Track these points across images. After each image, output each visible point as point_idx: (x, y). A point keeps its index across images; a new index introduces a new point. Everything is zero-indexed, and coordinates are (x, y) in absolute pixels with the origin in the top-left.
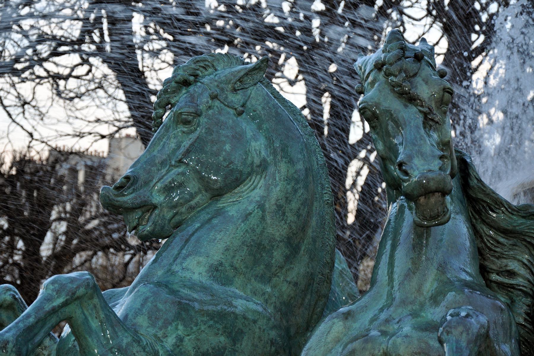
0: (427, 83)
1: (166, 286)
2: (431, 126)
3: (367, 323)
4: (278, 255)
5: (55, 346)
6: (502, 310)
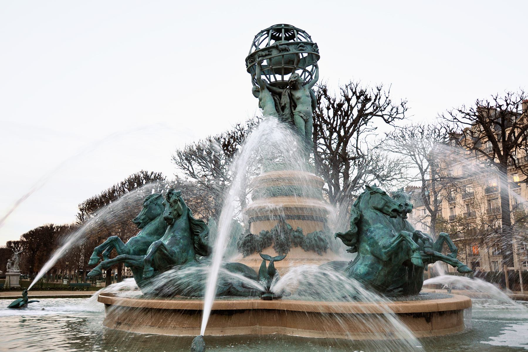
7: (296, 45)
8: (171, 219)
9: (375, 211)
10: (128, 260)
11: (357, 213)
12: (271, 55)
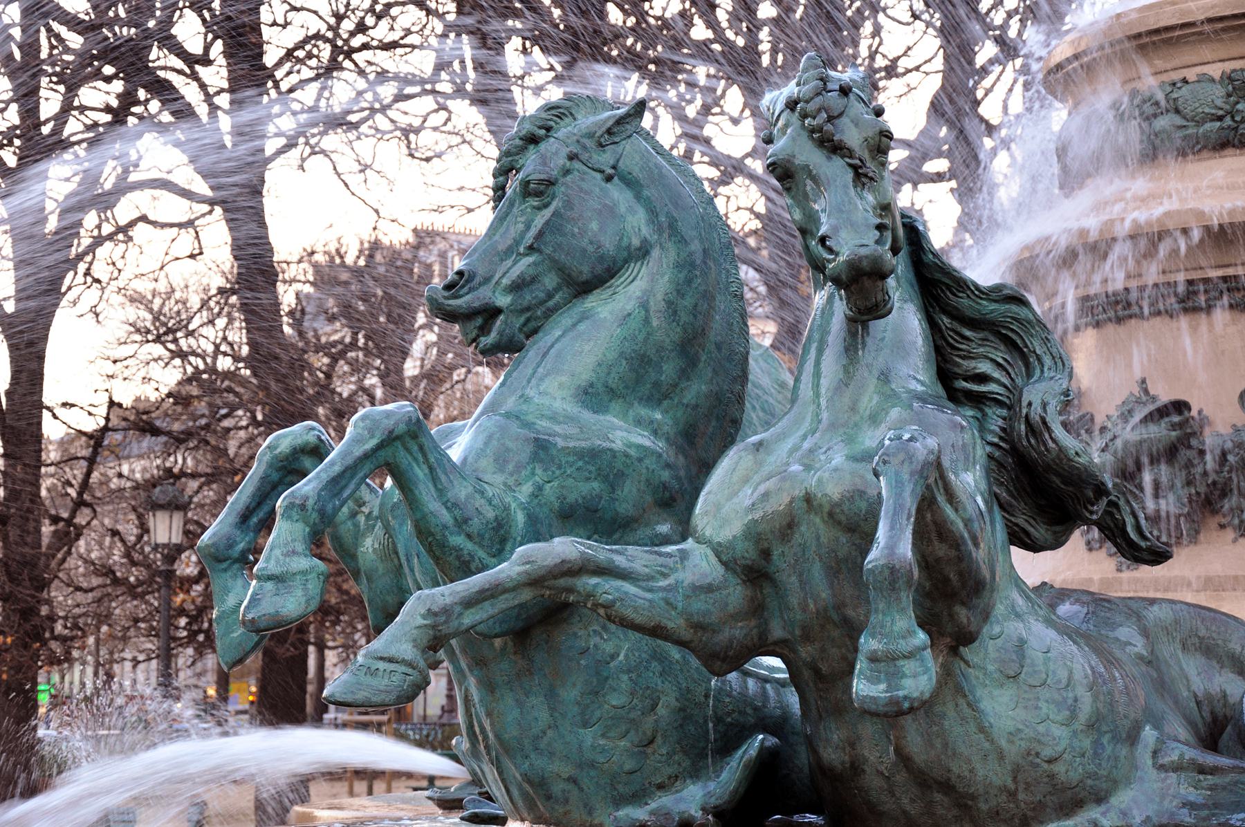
0: (856, 125)
1: (518, 418)
2: (864, 184)
3: (785, 456)
4: (669, 370)
5: (378, 501)
6: (962, 427)
10: (594, 580)
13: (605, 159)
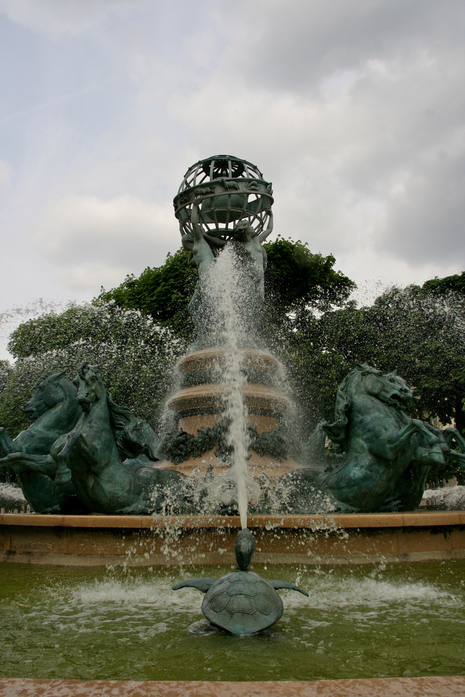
7: (247, 183)
8: (88, 403)
9: (369, 396)
11: (347, 398)
12: (214, 193)
13: (56, 382)
